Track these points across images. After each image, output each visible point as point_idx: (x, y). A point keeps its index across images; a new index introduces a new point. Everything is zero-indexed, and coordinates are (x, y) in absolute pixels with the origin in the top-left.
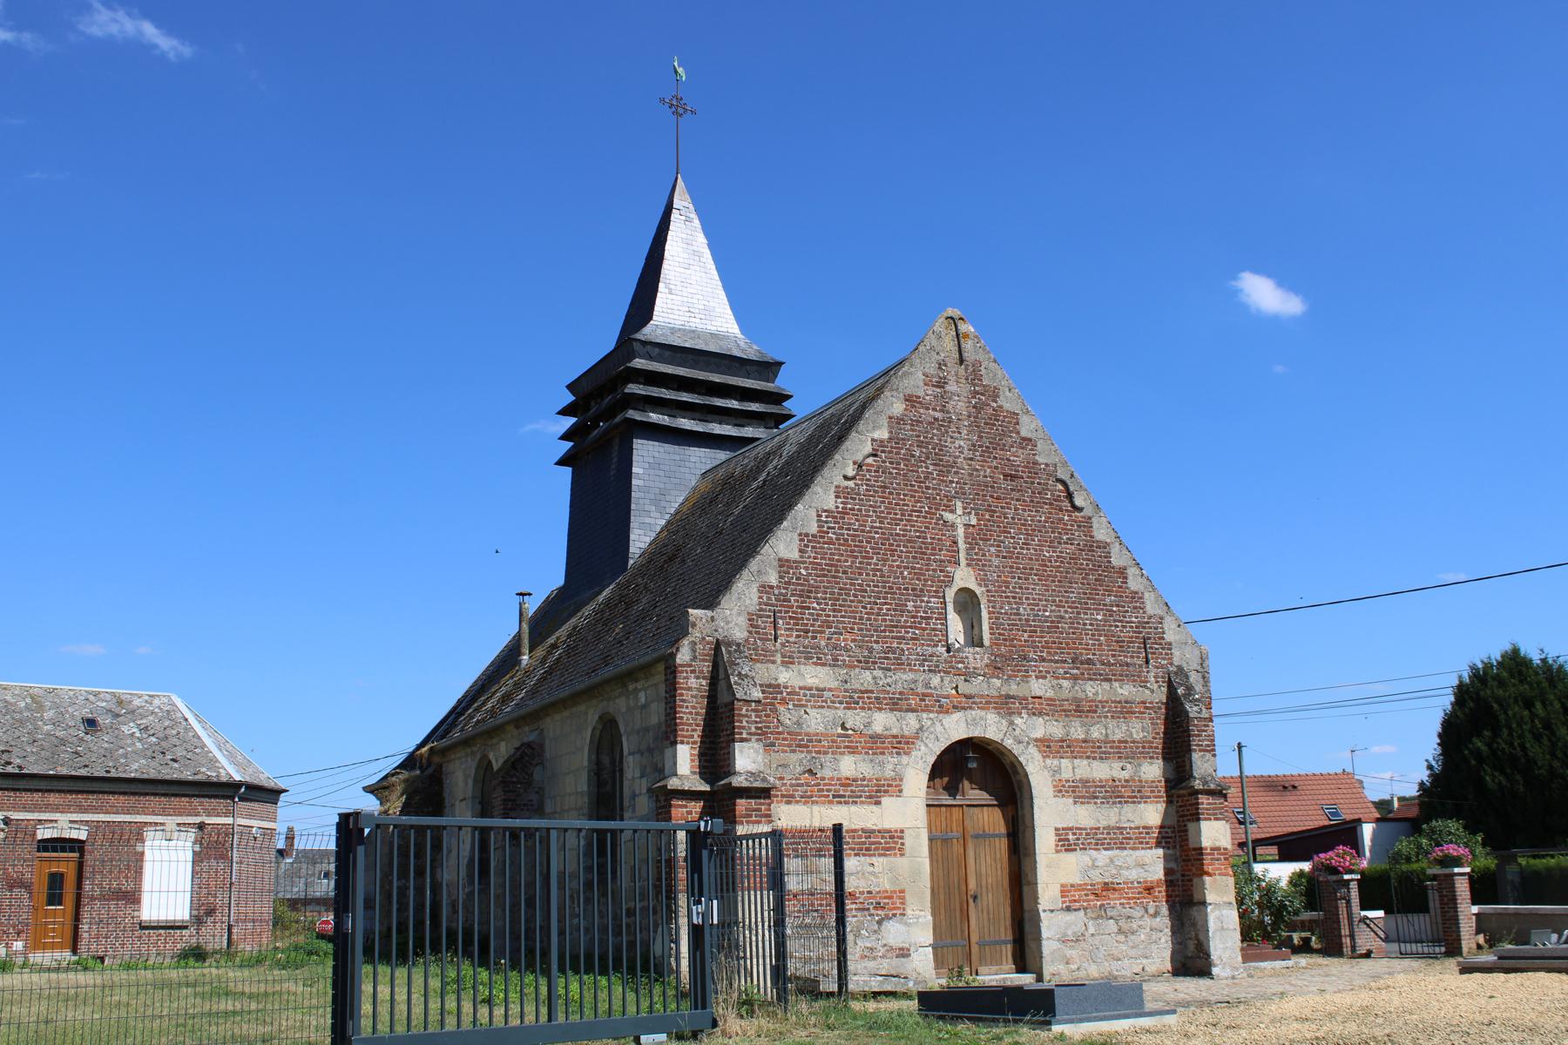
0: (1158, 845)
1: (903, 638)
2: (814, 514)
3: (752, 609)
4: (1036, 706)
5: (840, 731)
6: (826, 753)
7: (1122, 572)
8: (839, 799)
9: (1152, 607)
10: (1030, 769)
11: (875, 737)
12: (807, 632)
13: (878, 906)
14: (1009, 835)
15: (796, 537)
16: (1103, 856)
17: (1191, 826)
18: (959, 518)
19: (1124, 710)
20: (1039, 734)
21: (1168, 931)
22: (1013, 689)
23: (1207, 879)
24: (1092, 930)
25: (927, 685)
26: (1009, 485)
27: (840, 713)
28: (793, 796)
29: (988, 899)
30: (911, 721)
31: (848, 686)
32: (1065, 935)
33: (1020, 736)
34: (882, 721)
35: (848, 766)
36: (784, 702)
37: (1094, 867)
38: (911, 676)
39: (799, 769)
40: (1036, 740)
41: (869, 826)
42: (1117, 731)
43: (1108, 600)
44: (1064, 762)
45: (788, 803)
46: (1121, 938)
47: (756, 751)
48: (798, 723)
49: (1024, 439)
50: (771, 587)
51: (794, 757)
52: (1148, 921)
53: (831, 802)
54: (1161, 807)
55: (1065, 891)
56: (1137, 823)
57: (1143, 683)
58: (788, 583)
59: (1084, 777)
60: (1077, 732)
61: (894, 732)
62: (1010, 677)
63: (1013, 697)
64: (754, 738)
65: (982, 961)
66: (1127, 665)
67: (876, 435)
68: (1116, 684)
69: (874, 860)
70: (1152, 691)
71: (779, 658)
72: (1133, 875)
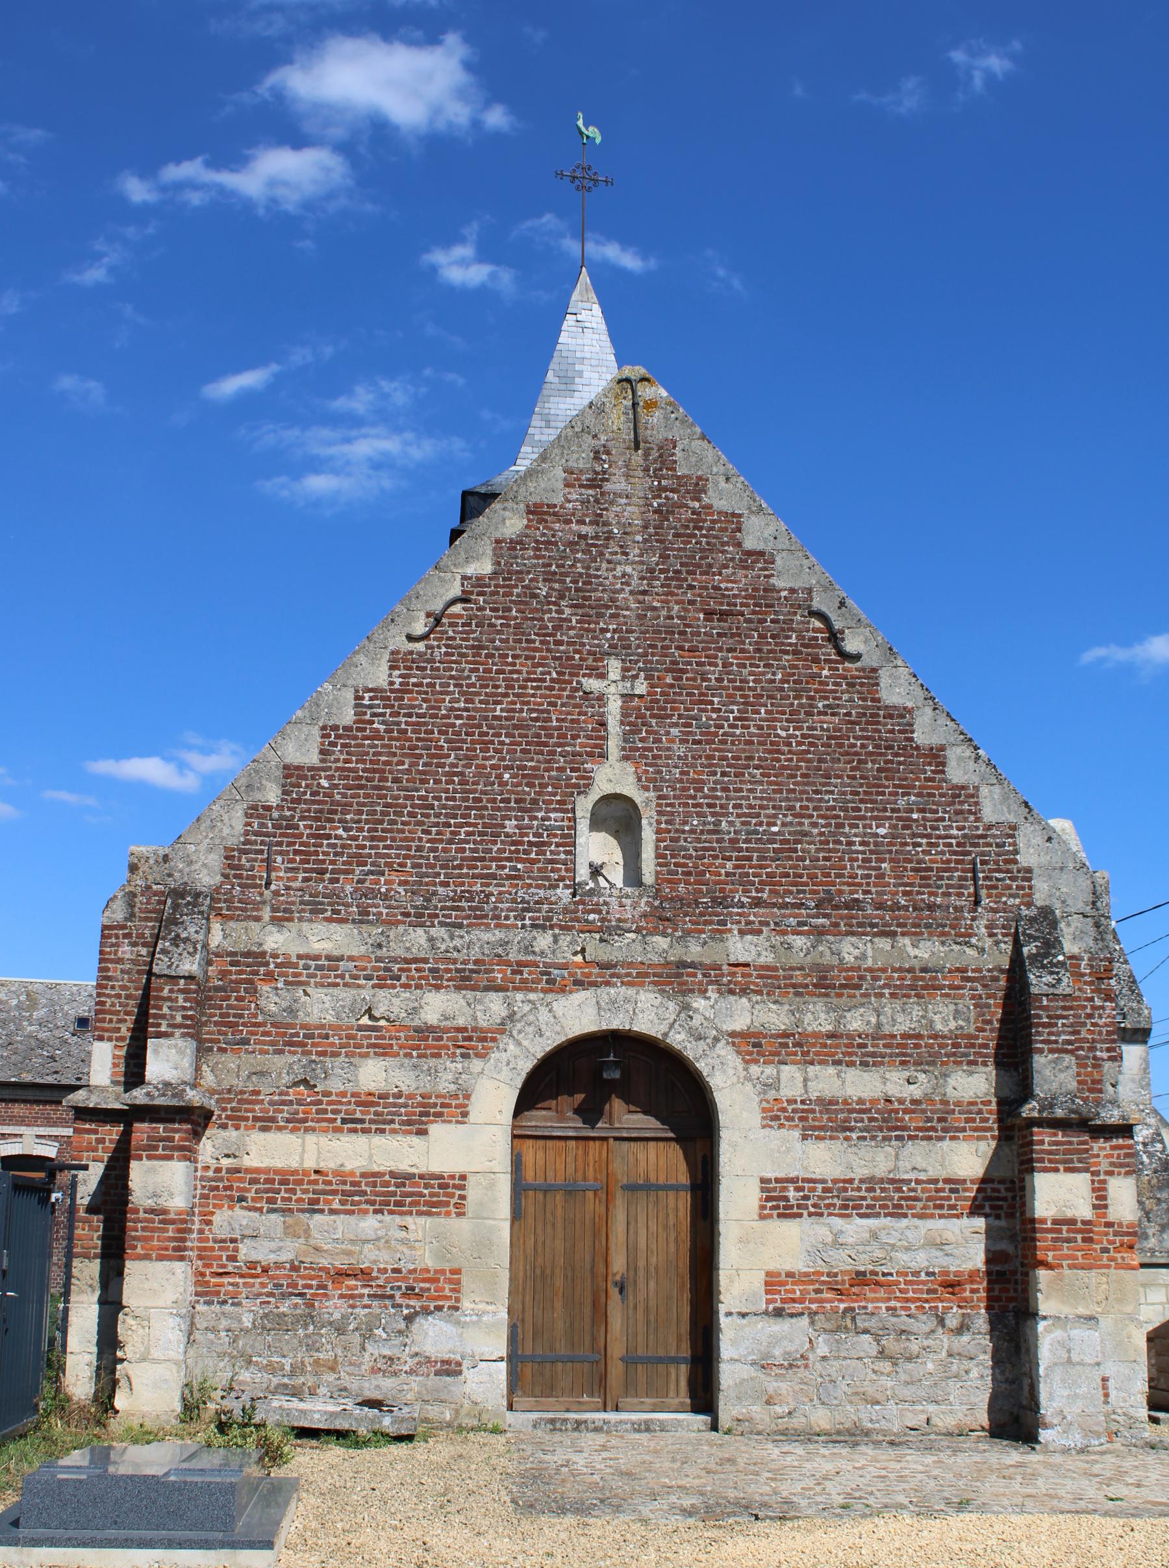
0: (975, 1210)
2: (350, 695)
3: (232, 842)
4: (737, 981)
5: (365, 1020)
6: (335, 1055)
7: (936, 756)
8: (352, 1124)
9: (993, 807)
11: (425, 1032)
12: (323, 872)
13: (410, 1292)
14: (694, 1188)
15: (316, 732)
16: (855, 1228)
17: (1027, 1178)
18: (612, 687)
19: (920, 983)
20: (740, 1023)
21: (986, 1359)
22: (694, 951)
23: (1042, 1274)
24: (822, 1349)
25: (528, 949)
26: (716, 627)
27: (366, 994)
28: (273, 1120)
29: (647, 1290)
30: (494, 1006)
31: (383, 952)
32: (768, 1355)
33: (707, 1032)
34: (438, 1006)
35: (374, 1074)
36: (270, 977)
37: (837, 1244)
38: (499, 934)
39: (286, 1079)
40: (733, 1034)
41: (404, 1167)
42: (903, 1019)
43: (902, 802)
44: (786, 1069)
45: (264, 1129)
46: (886, 1366)
47: (181, 1052)
48: (291, 1011)
49: (749, 553)
50: (268, 808)
51: (279, 1061)
52: (944, 1340)
53: (337, 1130)
54: (987, 1147)
55: (773, 1282)
56: (932, 1173)
57: (964, 938)
58: (298, 801)
59: (828, 1095)
60: (818, 1018)
61: (461, 1022)
62: (687, 933)
63: (692, 965)
64: (178, 1032)
65: (630, 1387)
66: (931, 907)
67: (470, 570)
68: (907, 941)
69: (409, 1220)
70: (982, 951)
71: (266, 914)
72: (920, 1260)
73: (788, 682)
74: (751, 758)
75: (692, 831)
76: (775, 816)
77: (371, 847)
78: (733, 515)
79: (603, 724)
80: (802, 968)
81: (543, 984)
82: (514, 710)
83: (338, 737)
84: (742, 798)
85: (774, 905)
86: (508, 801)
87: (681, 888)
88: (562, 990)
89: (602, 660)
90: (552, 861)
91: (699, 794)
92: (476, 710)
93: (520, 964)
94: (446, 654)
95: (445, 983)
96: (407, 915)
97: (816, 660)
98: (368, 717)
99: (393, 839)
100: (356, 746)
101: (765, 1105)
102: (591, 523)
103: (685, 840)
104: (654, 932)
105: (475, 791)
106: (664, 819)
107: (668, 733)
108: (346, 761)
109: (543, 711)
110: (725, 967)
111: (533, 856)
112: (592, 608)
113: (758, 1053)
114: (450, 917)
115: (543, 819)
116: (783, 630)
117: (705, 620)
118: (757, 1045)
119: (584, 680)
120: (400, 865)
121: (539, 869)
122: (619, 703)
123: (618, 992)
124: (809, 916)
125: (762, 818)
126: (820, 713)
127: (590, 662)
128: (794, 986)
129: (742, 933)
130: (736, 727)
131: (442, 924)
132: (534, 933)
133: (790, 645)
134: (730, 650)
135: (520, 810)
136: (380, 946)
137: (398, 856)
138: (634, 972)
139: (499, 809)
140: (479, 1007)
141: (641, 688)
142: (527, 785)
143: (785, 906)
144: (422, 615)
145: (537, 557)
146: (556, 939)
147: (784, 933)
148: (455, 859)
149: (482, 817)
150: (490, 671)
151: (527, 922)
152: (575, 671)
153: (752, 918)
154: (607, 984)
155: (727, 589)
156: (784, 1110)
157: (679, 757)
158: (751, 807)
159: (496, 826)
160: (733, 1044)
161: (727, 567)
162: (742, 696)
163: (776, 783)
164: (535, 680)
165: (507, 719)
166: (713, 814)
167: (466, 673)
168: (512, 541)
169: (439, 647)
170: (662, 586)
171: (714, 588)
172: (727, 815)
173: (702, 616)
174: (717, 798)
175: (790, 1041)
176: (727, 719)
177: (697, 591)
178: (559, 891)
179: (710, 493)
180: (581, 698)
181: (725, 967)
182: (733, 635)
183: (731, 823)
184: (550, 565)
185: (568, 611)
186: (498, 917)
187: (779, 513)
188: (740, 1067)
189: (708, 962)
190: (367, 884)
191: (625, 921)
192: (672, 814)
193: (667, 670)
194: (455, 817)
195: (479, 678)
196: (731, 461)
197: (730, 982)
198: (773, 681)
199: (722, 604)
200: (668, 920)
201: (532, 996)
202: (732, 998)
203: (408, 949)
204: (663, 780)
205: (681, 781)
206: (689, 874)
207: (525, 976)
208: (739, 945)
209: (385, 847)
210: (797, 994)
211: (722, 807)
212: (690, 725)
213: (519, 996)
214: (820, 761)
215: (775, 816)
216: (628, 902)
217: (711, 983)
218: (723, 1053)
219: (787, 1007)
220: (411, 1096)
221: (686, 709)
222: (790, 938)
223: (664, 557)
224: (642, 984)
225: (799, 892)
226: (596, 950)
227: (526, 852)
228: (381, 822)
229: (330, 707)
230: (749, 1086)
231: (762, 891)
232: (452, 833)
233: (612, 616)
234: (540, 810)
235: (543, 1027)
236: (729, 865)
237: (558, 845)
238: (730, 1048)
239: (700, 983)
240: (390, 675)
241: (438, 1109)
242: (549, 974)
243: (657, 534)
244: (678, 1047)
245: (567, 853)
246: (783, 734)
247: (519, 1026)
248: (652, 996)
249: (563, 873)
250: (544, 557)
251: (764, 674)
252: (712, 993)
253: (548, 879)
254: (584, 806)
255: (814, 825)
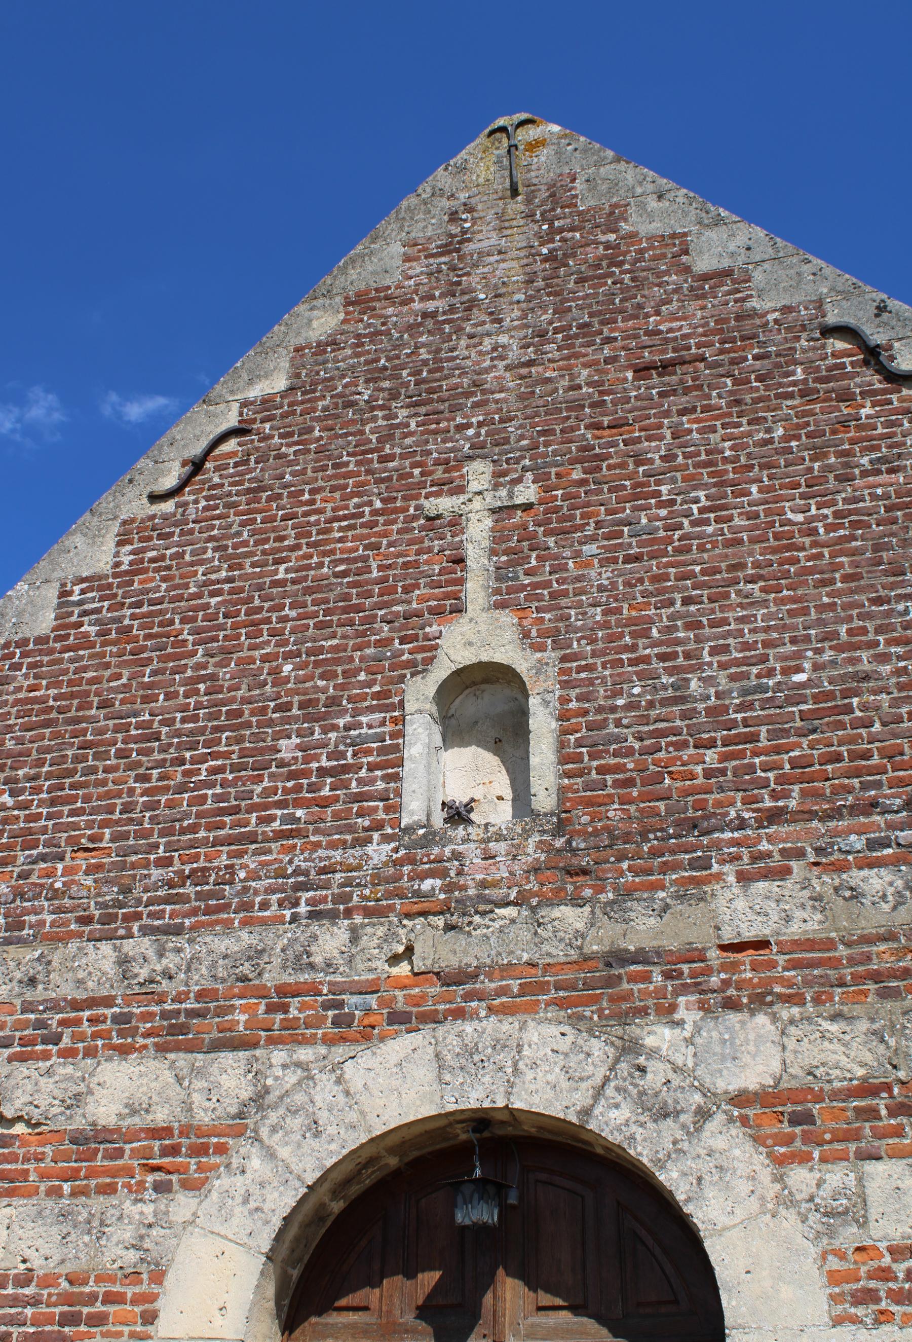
1: (252, 838)
2: (51, 593)
4: (743, 976)
10: (708, 1213)
11: (92, 1141)
18: (475, 508)
20: (756, 1070)
22: (644, 928)
25: (301, 960)
30: (229, 1078)
34: (123, 1088)
40: (741, 1099)
61: (160, 1116)
62: (628, 892)
73: (798, 438)
74: (742, 566)
75: (631, 706)
76: (799, 655)
77: (49, 817)
78: (674, 236)
79: (460, 561)
80: (890, 937)
81: (328, 1028)
82: (308, 568)
83: (24, 655)
84: (729, 634)
85: (812, 815)
86: (287, 707)
87: (614, 812)
88: (366, 1036)
89: (458, 468)
90: (359, 798)
91: (641, 642)
92: (245, 577)
93: (284, 991)
94: (206, 509)
95: (141, 1041)
96: (86, 920)
97: (846, 397)
98: (74, 619)
99: (87, 799)
100: (51, 663)
101: (834, 1263)
102: (442, 295)
103: (618, 723)
104: (558, 898)
105: (232, 700)
106: (573, 693)
107: (578, 554)
108: (31, 689)
109: (355, 560)
110: (713, 954)
111: (326, 792)
112: (434, 398)
113: (807, 1138)
114: (159, 915)
115: (347, 728)
116: (778, 365)
117: (635, 379)
118: (803, 1119)
119: (426, 503)
120: (92, 839)
121: (336, 816)
122: (489, 522)
123: (482, 1029)
124: (890, 826)
125: (772, 663)
126: (865, 474)
127: (439, 474)
128: (876, 976)
129: (744, 878)
130: (707, 522)
131: (146, 931)
132: (315, 928)
133: (794, 384)
134: (682, 412)
135: (307, 718)
136: (32, 981)
137: (90, 825)
138: (515, 985)
139: (271, 723)
140: (199, 1084)
141: (528, 492)
142: (322, 677)
143: (836, 813)
144: (177, 464)
145: (357, 355)
146: (355, 935)
147: (840, 868)
148: (187, 815)
149: (240, 740)
150: (273, 519)
151: (303, 909)
152: (413, 492)
153: (765, 846)
154: (459, 1014)
155: (670, 330)
156: (885, 1274)
157: (601, 589)
158: (746, 647)
159: (262, 751)
160: (744, 1121)
161: (669, 302)
162: (711, 475)
163: (793, 600)
164: (345, 518)
165: (294, 582)
166: (670, 672)
167: (235, 528)
168: (319, 344)
169: (196, 502)
170: (559, 349)
171: (648, 333)
172: (700, 667)
173: (630, 375)
174: (678, 642)
175: (881, 1104)
176: (688, 514)
177: (619, 344)
178: (370, 849)
179: (634, 218)
180: (422, 529)
181: (713, 954)
182: (687, 391)
183: (708, 681)
184: (377, 360)
185: (403, 413)
186: (246, 907)
187: (750, 217)
188: (765, 1175)
189: (673, 945)
190: (34, 879)
191: (495, 884)
192: (591, 682)
193: (573, 462)
194: (193, 747)
195: (253, 533)
196: (663, 175)
197: (726, 983)
198: (770, 441)
199: (664, 352)
200: (585, 872)
201: (305, 1054)
202: (733, 1018)
203: (80, 982)
204: (570, 629)
205: (606, 625)
206: (629, 783)
207: (293, 1012)
208: (741, 904)
209: (72, 813)
210: (885, 994)
211: (687, 656)
212: (620, 534)
213: (279, 1056)
214: (877, 548)
215: (799, 655)
216: (500, 848)
217: (684, 989)
218: (720, 1143)
219: (863, 1026)
220: (48, 1281)
221: (609, 512)
222: (855, 876)
223: (562, 311)
224: (532, 1009)
225: (865, 787)
226: (435, 947)
227: (312, 788)
228: (71, 773)
229: (20, 614)
230: (789, 1220)
231: (787, 795)
232: (186, 773)
233: (476, 405)
234: (342, 713)
235: (323, 1117)
236: (710, 756)
237: (371, 768)
238: (736, 1130)
239: (660, 993)
240: (117, 554)
241: (99, 1307)
242: (340, 1005)
243: (548, 286)
244: (615, 1138)
245: (387, 778)
246: (800, 518)
247: (273, 1117)
248: (555, 1030)
249: (381, 815)
250: (368, 352)
251: (749, 434)
252: (687, 1010)
253: (351, 829)
254: (419, 693)
255: (884, 658)
